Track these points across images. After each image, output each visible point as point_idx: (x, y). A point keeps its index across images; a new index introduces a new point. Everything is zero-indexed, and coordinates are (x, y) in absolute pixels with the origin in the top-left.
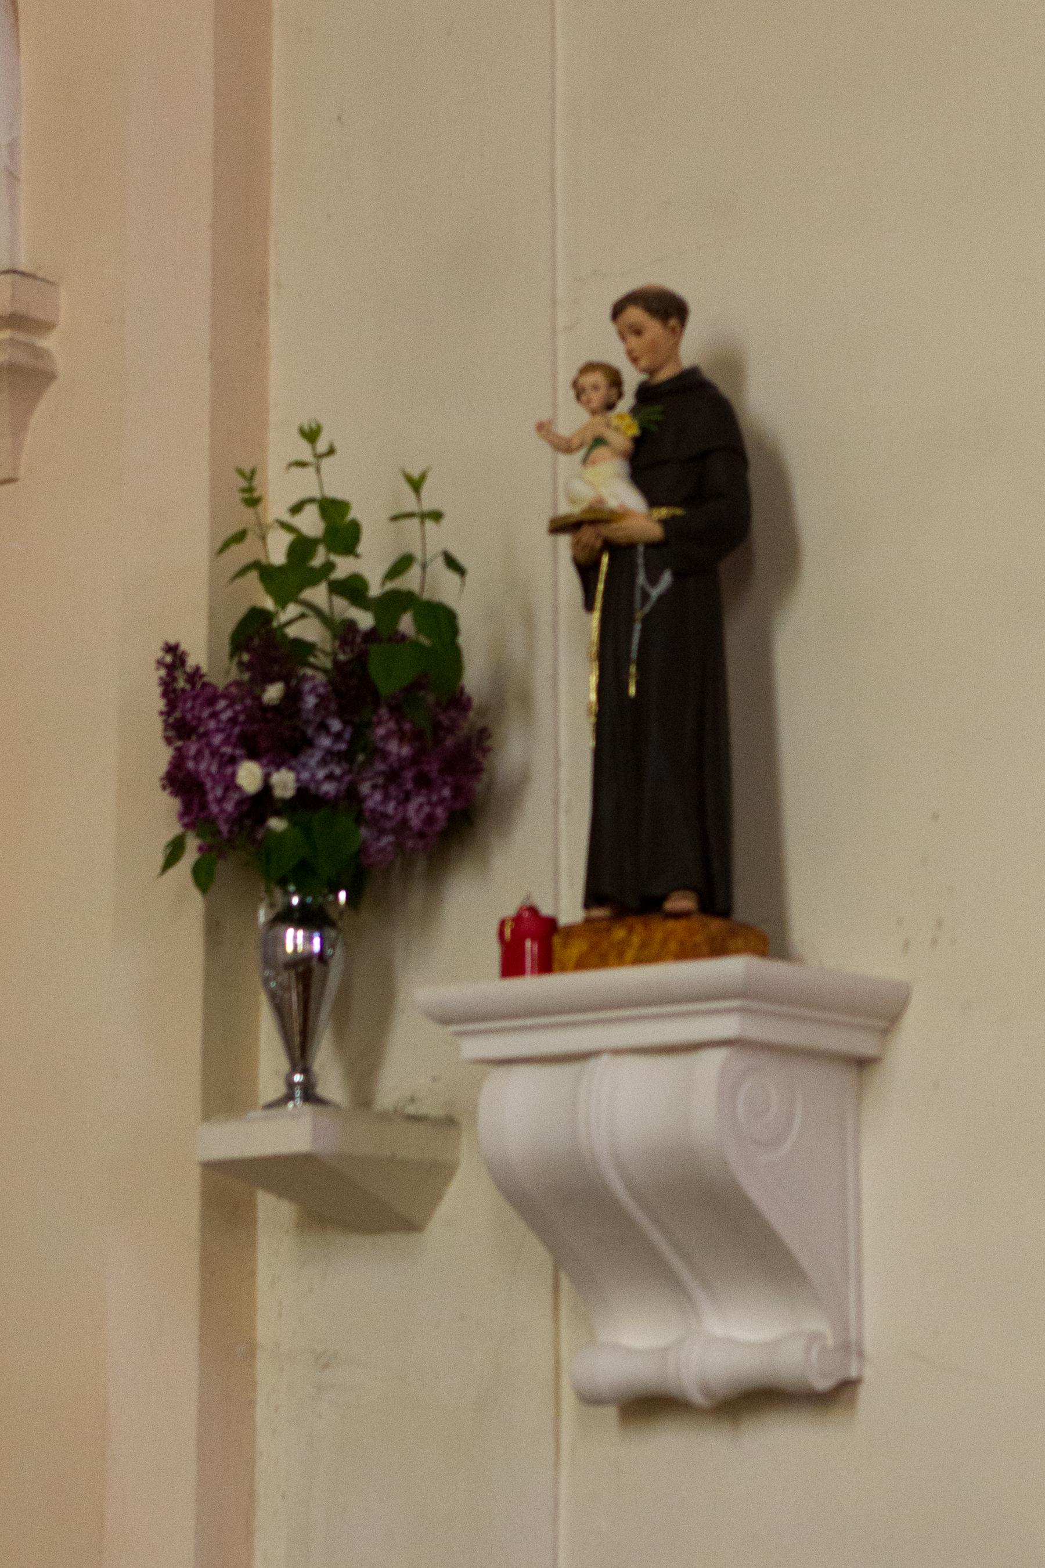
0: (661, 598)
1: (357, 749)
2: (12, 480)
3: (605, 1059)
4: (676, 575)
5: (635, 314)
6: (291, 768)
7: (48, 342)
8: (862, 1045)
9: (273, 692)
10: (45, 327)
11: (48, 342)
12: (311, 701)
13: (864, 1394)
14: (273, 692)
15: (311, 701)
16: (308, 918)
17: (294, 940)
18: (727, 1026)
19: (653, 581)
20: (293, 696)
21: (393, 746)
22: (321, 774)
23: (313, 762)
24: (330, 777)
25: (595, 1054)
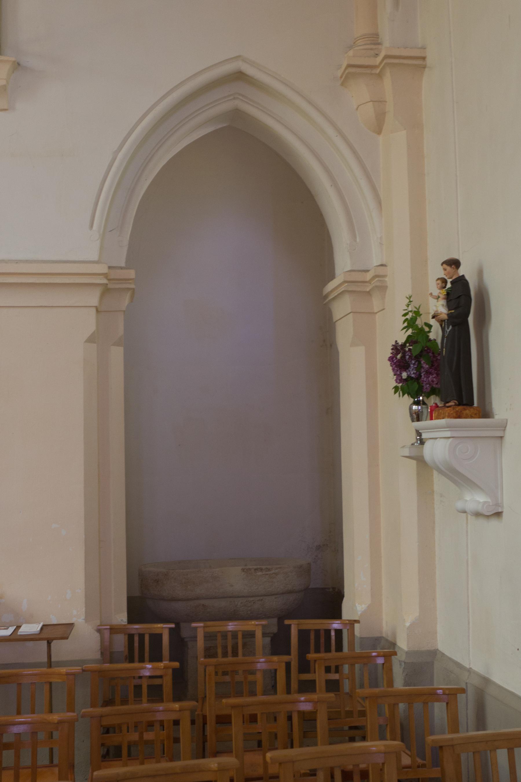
0: (449, 332)
1: (419, 367)
2: (384, 309)
3: (438, 439)
4: (453, 326)
5: (445, 265)
6: (407, 372)
7: (386, 279)
8: (499, 434)
9: (399, 357)
10: (385, 276)
11: (386, 279)
12: (407, 357)
13: (504, 514)
14: (399, 357)
15: (407, 357)
16: (417, 403)
17: (415, 407)
18: (448, 434)
19: (448, 328)
20: (403, 357)
21: (424, 366)
22: (412, 373)
23: (411, 370)
24: (414, 373)
25: (437, 438)
